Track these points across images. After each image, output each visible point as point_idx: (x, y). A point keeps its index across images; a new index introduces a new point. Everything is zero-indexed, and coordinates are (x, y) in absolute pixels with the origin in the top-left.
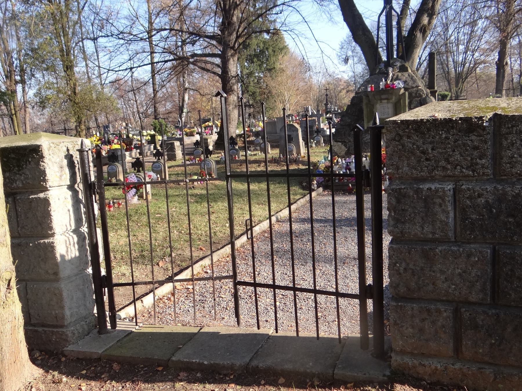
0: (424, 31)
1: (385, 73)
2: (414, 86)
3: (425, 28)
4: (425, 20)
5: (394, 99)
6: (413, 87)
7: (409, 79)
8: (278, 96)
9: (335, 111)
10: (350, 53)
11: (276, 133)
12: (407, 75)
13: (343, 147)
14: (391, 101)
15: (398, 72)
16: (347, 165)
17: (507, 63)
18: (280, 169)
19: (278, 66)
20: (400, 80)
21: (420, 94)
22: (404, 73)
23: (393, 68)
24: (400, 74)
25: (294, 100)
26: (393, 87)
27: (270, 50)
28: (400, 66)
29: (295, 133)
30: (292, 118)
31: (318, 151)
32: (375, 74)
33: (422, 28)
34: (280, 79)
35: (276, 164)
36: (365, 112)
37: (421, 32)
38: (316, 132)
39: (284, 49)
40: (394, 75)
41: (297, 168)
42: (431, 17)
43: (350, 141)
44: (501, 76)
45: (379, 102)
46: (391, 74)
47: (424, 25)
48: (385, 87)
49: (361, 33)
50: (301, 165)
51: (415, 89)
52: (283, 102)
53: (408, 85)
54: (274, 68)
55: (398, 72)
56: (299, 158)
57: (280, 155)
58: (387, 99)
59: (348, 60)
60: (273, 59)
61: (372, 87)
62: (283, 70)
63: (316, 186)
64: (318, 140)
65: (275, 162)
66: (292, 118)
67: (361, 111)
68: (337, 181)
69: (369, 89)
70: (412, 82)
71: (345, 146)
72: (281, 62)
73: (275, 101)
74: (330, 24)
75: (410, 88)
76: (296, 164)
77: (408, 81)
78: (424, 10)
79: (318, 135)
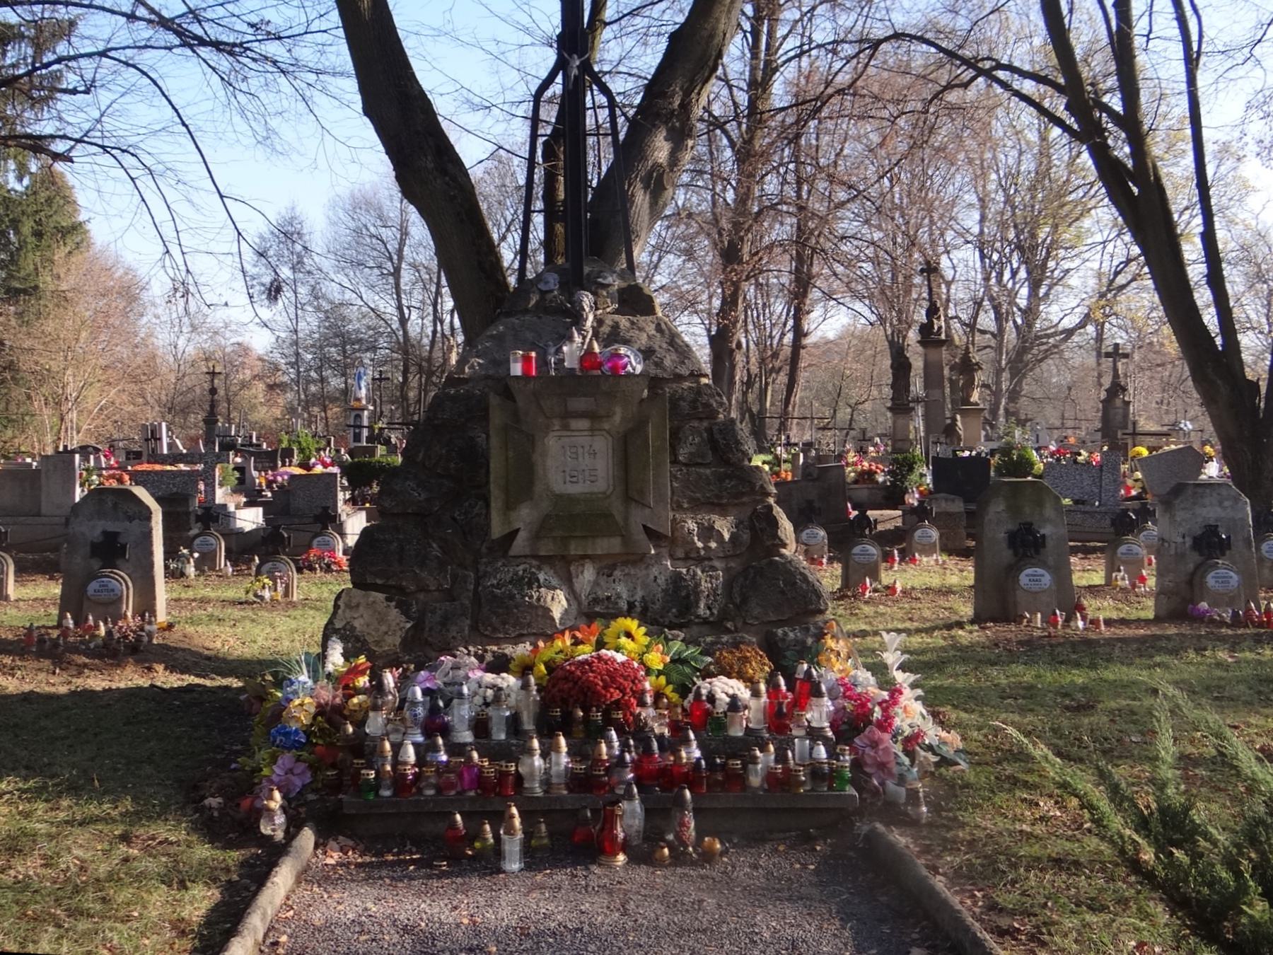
0: (657, 185)
1: (567, 313)
2: (684, 371)
3: (661, 176)
4: (660, 149)
5: (617, 418)
6: (679, 378)
7: (660, 343)
8: (42, 382)
9: (251, 445)
10: (285, 272)
11: (39, 515)
12: (651, 329)
13: (394, 614)
14: (606, 426)
15: (616, 312)
16: (433, 711)
17: (739, 345)
18: (63, 690)
19: (46, 281)
20: (626, 342)
21: (708, 405)
22: (641, 320)
23: (594, 294)
24: (624, 321)
25: (93, 398)
26: (615, 369)
27: (27, 227)
28: (621, 291)
29: (135, 527)
30: (97, 460)
31: (208, 592)
32: (526, 311)
33: (650, 174)
34: (50, 326)
35: (47, 663)
36: (496, 464)
37: (646, 188)
38: (199, 518)
39: (73, 231)
40: (599, 321)
41: (144, 682)
42: (679, 137)
43: (424, 589)
44: (726, 378)
45: (557, 424)
46: (591, 317)
47: (657, 166)
48: (582, 367)
49: (431, 166)
50: (160, 668)
51: (686, 384)
52: (58, 404)
53: (659, 364)
54: (36, 288)
55: (616, 312)
56: (150, 635)
57: (62, 617)
58: (592, 416)
59: (278, 290)
60: (30, 261)
61: (527, 360)
62: (63, 299)
63: (280, 819)
64: (205, 549)
65: (40, 655)
66: (97, 460)
67: (475, 459)
68: (386, 793)
69: (517, 369)
70: (674, 357)
71: (404, 608)
72: (62, 273)
73: (29, 397)
74: (260, 152)
75: (667, 380)
76: (137, 662)
77: (660, 353)
78: (658, 115)
79: (205, 531)
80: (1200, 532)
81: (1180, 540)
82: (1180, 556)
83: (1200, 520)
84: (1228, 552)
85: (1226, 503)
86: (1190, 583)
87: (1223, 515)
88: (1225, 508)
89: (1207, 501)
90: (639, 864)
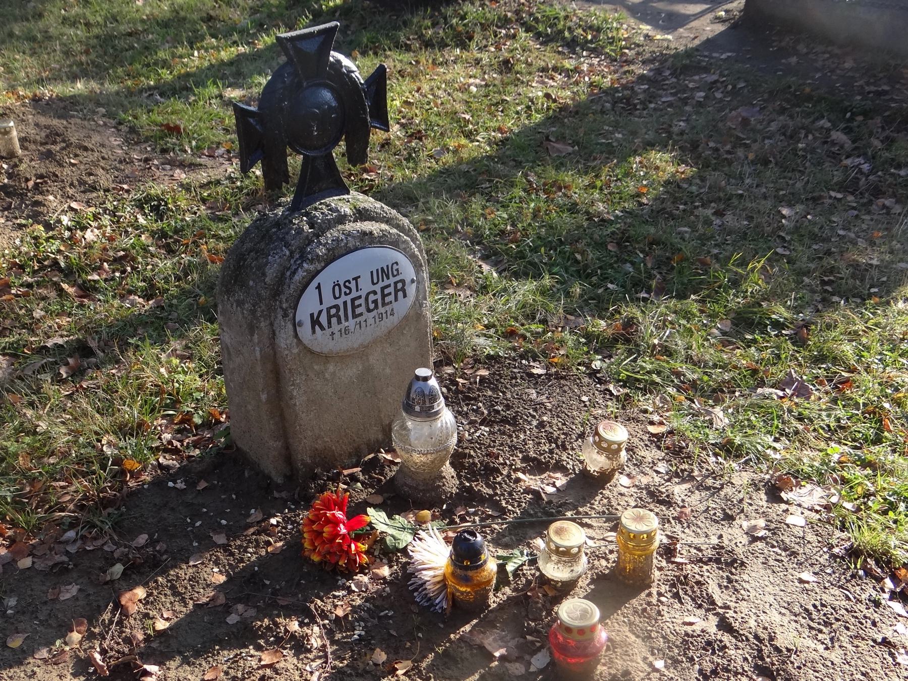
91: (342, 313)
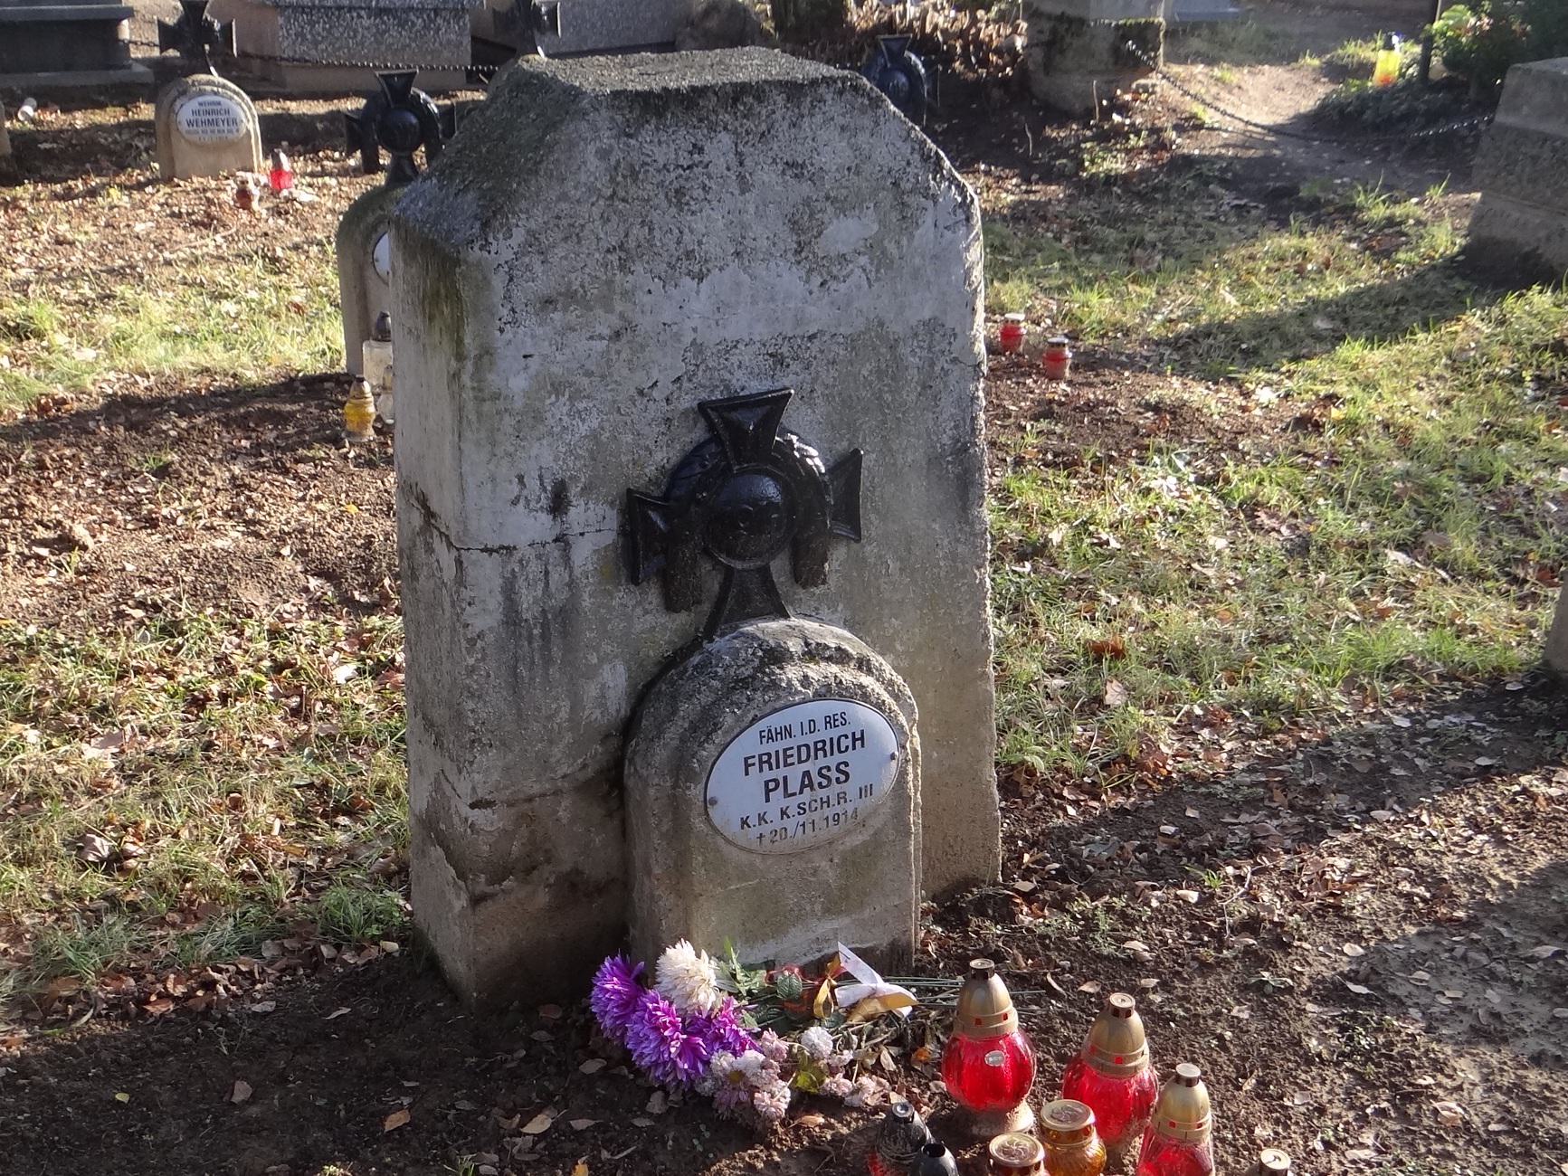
80: (664, 456)
81: (533, 526)
82: (544, 634)
83: (665, 366)
84: (837, 560)
85: (844, 233)
86: (610, 785)
87: (819, 315)
88: (825, 270)
89: (709, 226)
90: (622, 512)
91: (773, 760)
